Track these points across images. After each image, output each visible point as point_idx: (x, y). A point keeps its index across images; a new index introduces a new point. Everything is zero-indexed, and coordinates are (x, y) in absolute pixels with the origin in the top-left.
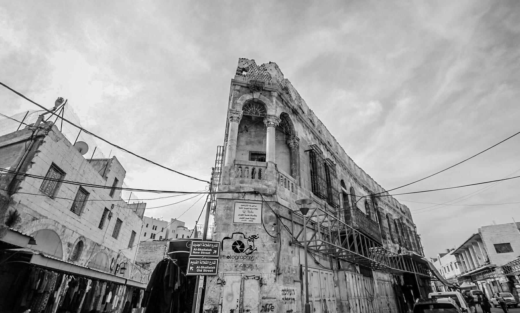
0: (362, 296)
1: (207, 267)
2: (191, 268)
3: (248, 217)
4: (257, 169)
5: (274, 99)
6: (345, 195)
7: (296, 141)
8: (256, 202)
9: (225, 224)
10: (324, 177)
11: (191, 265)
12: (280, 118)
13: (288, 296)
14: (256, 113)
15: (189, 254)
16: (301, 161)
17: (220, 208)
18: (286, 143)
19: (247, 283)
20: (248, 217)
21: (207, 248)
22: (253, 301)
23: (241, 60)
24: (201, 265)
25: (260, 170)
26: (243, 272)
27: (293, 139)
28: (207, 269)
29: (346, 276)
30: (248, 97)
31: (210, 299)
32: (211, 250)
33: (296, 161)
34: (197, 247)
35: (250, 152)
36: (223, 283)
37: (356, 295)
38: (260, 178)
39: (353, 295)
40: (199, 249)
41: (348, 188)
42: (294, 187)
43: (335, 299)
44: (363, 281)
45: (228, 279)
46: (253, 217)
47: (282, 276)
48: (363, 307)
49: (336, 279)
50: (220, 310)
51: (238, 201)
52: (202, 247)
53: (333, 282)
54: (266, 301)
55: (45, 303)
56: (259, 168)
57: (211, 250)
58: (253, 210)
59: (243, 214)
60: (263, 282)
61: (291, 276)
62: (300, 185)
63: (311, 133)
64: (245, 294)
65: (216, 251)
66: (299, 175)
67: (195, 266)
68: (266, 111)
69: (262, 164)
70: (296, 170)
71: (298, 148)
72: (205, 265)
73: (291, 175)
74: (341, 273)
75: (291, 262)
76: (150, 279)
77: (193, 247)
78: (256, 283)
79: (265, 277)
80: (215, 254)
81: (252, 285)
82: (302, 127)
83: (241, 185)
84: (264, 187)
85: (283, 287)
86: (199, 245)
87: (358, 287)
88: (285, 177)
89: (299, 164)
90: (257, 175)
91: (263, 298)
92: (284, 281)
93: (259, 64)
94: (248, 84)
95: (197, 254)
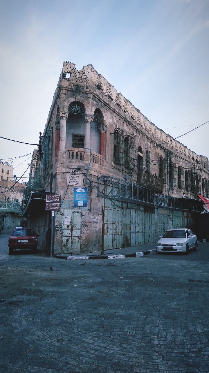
0: (141, 223)
3: (74, 182)
5: (91, 100)
6: (140, 158)
7: (105, 128)
9: (63, 186)
11: (47, 206)
12: (94, 115)
13: (95, 221)
14: (78, 111)
15: (46, 201)
16: (107, 142)
17: (59, 178)
18: (98, 128)
19: (75, 215)
21: (54, 198)
22: (78, 222)
23: (66, 63)
25: (81, 153)
26: (72, 209)
27: (102, 126)
29: (130, 212)
30: (72, 100)
31: (57, 221)
33: (104, 143)
34: (49, 198)
35: (73, 134)
36: (63, 214)
37: (136, 222)
38: (81, 159)
39: (134, 221)
41: (144, 151)
42: (102, 161)
43: (122, 223)
44: (143, 216)
45: (66, 213)
46: (77, 182)
47: (92, 212)
48: (140, 229)
49: (124, 213)
50: (62, 225)
51: (68, 173)
53: (122, 215)
56: (80, 152)
57: (56, 199)
60: (83, 214)
61: (97, 212)
62: (106, 159)
63: (117, 116)
64: (74, 219)
66: (106, 152)
67: (49, 207)
68: (84, 113)
69: (82, 150)
70: (103, 149)
71: (106, 133)
72: (54, 206)
73: (100, 154)
74: (128, 211)
75: (97, 205)
76: (164, 260)
77: (47, 198)
78: (79, 215)
79: (84, 212)
80: (58, 201)
81: (77, 215)
82: (110, 114)
83: (70, 164)
84: (83, 165)
85: (92, 217)
87: (139, 218)
88: (95, 156)
89: (106, 145)
90: (79, 157)
91: (83, 221)
92: (93, 214)
93: (79, 68)
94: (72, 89)
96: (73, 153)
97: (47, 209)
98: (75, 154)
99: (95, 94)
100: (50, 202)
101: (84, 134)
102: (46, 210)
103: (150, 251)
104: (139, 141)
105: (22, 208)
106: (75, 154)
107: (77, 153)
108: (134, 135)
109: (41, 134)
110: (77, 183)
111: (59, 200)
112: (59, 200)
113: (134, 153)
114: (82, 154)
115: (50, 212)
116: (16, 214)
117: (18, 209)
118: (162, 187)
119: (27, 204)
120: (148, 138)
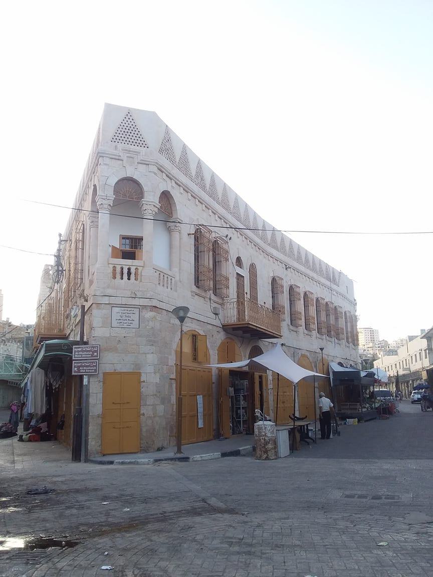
2: (76, 369)
3: (125, 321)
6: (239, 276)
11: (75, 367)
20: (125, 321)
21: (88, 351)
24: (83, 366)
32: (91, 353)
34: (79, 351)
52: (83, 351)
54: (228, 424)
56: (128, 267)
65: (96, 354)
72: (87, 366)
80: (95, 356)
86: (80, 349)
96: (122, 269)
97: (75, 372)
98: (125, 271)
99: (161, 166)
100: (91, 359)
101: (141, 235)
102: (73, 374)
103: (239, 450)
104: (236, 247)
105: (20, 372)
106: (125, 271)
107: (129, 269)
108: (229, 237)
109: (60, 235)
111: (97, 354)
112: (97, 354)
113: (230, 270)
114: (139, 271)
115: (81, 377)
116: (12, 383)
117: (13, 373)
118: (279, 328)
119: (34, 363)
120: (256, 246)
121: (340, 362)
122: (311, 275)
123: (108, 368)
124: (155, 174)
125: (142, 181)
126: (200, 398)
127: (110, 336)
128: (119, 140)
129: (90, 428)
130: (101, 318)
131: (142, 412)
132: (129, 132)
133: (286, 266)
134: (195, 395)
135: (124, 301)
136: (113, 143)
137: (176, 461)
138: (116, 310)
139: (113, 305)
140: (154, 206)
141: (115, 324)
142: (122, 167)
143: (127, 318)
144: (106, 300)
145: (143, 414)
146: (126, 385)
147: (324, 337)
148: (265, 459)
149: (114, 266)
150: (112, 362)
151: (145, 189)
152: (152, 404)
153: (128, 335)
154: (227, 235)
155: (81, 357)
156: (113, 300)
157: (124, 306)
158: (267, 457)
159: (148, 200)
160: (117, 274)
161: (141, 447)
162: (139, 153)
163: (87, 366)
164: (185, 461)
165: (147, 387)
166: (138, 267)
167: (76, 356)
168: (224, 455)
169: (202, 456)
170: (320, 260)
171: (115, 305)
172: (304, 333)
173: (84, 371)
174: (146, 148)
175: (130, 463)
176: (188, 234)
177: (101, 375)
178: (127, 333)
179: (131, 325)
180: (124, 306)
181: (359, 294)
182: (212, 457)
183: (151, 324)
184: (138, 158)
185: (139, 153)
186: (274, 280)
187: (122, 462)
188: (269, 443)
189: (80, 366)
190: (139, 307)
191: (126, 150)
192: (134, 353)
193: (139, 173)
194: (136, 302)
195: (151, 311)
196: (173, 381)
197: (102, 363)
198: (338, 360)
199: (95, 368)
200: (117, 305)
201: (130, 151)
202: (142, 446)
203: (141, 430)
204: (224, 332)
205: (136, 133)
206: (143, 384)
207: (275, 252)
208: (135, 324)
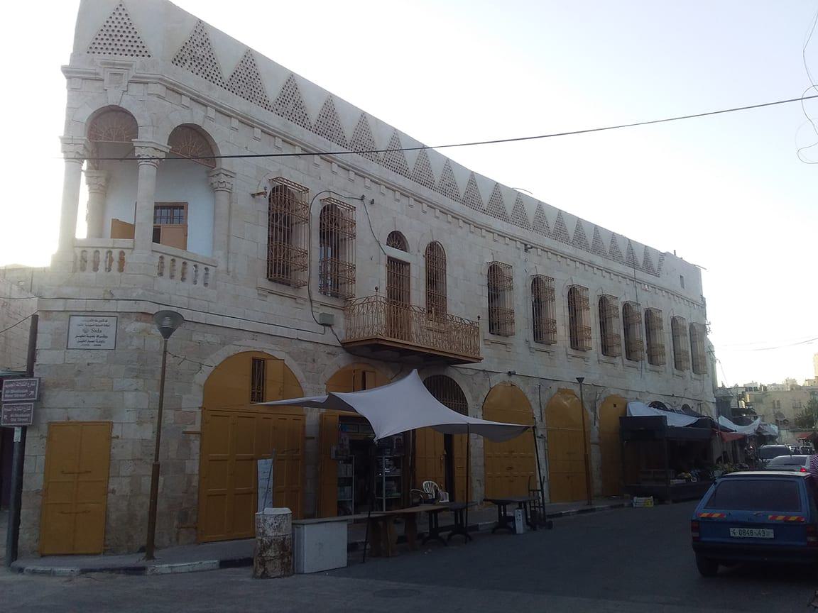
1: (22, 415)
2: (5, 416)
3: (91, 339)
4: (168, 260)
8: (93, 314)
10: (180, 269)
20: (91, 339)
25: (122, 254)
28: (22, 418)
32: (26, 391)
34: (10, 388)
40: (12, 391)
46: (101, 339)
52: (17, 388)
55: (775, 517)
57: (26, 391)
58: (100, 328)
59: (84, 334)
65: (32, 392)
67: (9, 414)
72: (19, 413)
86: (12, 385)
95: (10, 398)
97: (5, 421)
110: (99, 339)
111: (35, 393)
112: (35, 393)
118: (477, 348)
121: (656, 402)
122: (585, 259)
123: (58, 416)
124: (159, 97)
125: (134, 111)
126: (264, 466)
127: (64, 363)
128: (99, 44)
129: (22, 511)
130: (51, 334)
131: (111, 487)
132: (119, 34)
133: (526, 245)
134: (252, 459)
135: (90, 306)
136: (91, 54)
137: (119, 573)
138: (76, 320)
139: (71, 313)
140: (155, 149)
141: (73, 342)
142: (101, 91)
143: (96, 334)
144: (60, 305)
145: (113, 491)
146: (86, 445)
147: (618, 360)
148: (261, 577)
149: (85, 251)
150: (64, 405)
151: (140, 122)
152: (129, 474)
153: (94, 361)
154: (363, 196)
155: (14, 398)
156: (71, 305)
157: (90, 314)
158: (263, 573)
159: (143, 140)
160: (100, 263)
161: (105, 546)
162: (131, 66)
163: (19, 413)
164: (137, 574)
165: (122, 447)
166: (125, 251)
167: (6, 396)
168: (225, 564)
169: (175, 565)
170: (596, 228)
171: (75, 313)
172: (567, 354)
173: (15, 420)
174: (146, 57)
175: (43, 573)
176: (253, 195)
177: (44, 427)
178: (94, 359)
179: (102, 344)
180: (90, 314)
181: (711, 289)
182: (197, 568)
183: (136, 342)
184: (128, 74)
185: (131, 66)
186: (494, 270)
187: (33, 570)
188: (269, 547)
189: (12, 412)
190: (117, 314)
191: (108, 64)
192: (103, 390)
193: (132, 101)
194: (111, 306)
195: (137, 320)
196: (191, 435)
197: (49, 408)
198: (652, 399)
199: (28, 415)
200: (77, 313)
201: (114, 64)
202: (107, 543)
203: (107, 517)
204: (348, 354)
205: (130, 35)
206: (115, 441)
207: (498, 224)
208: (109, 343)
